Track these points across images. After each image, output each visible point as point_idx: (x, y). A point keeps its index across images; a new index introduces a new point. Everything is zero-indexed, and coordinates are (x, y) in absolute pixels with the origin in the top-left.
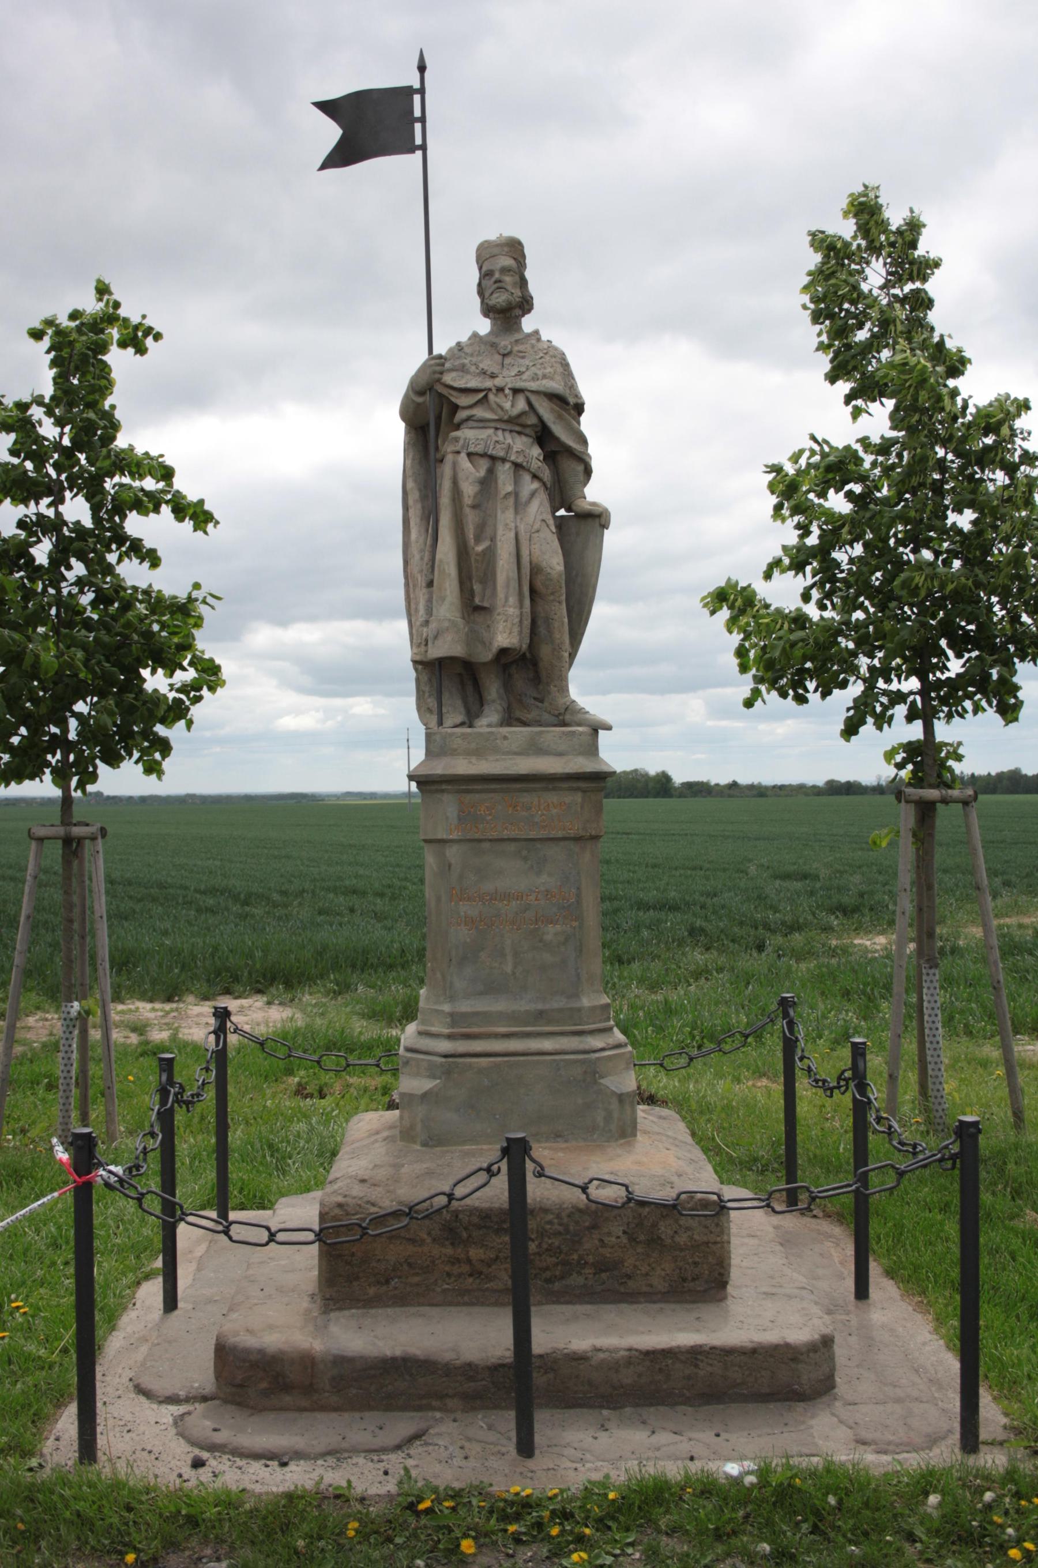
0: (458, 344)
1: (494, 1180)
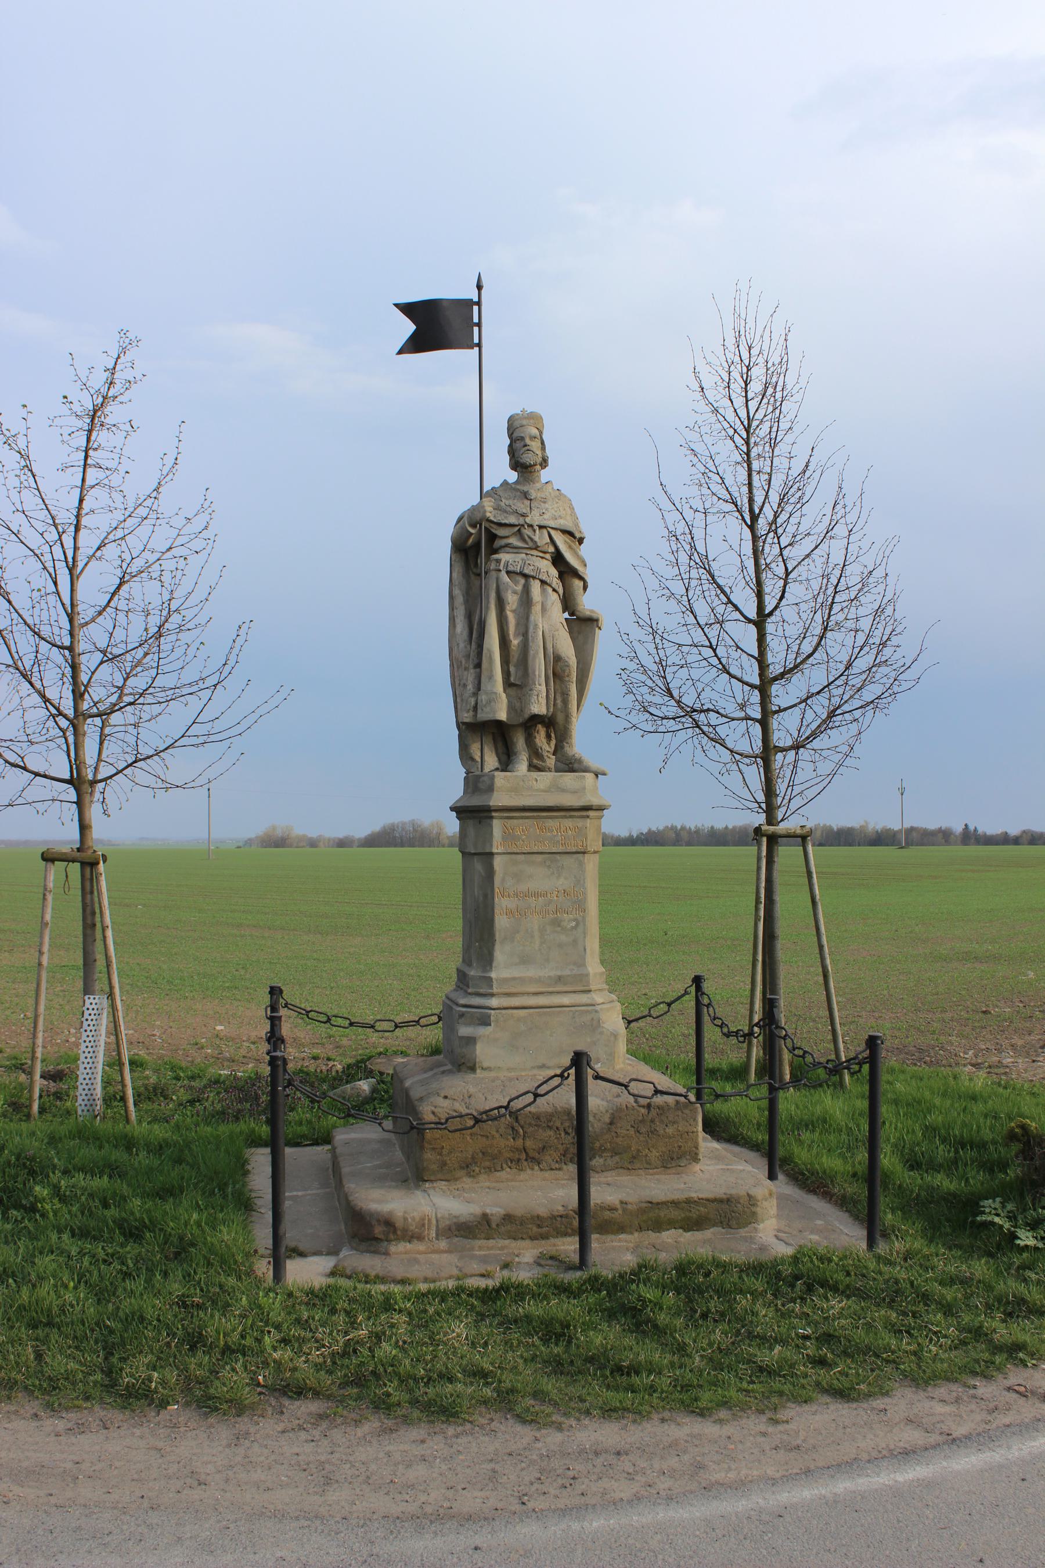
1: (565, 1082)
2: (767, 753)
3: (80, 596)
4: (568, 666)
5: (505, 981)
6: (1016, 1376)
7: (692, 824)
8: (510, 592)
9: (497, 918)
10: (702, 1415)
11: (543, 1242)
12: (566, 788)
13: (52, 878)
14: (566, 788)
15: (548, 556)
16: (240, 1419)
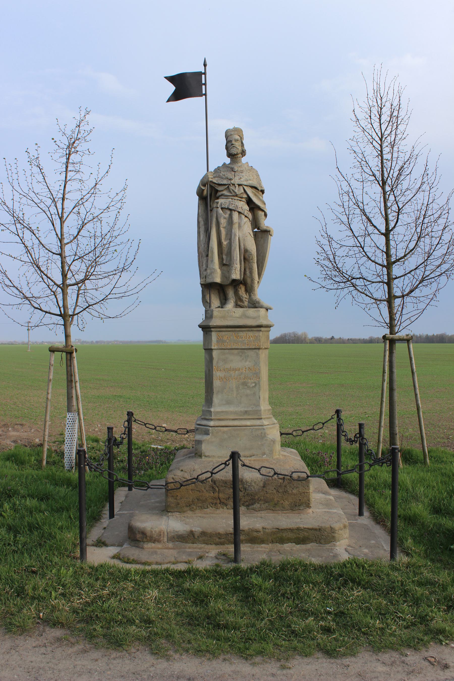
2: (390, 300)
3: (65, 230)
4: (251, 254)
5: (218, 413)
6: (434, 651)
7: (430, 334)
8: (222, 218)
10: (246, 659)
11: (222, 546)
12: (250, 316)
13: (53, 359)
14: (250, 316)
15: (244, 200)
16: (20, 637)
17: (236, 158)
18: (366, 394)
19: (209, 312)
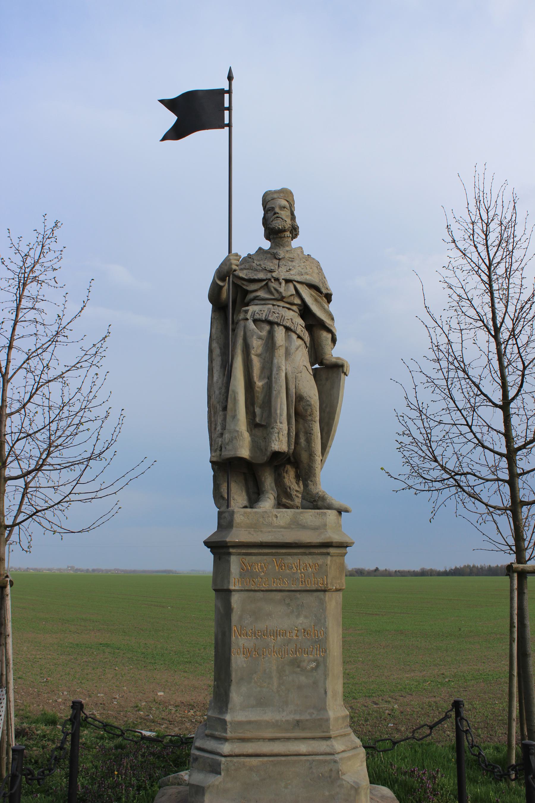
0: (249, 255)
4: (310, 405)
5: (240, 724)
7: (478, 564)
8: (255, 337)
9: (233, 657)
12: (309, 525)
17: (281, 237)
18: (435, 644)
19: (226, 515)
